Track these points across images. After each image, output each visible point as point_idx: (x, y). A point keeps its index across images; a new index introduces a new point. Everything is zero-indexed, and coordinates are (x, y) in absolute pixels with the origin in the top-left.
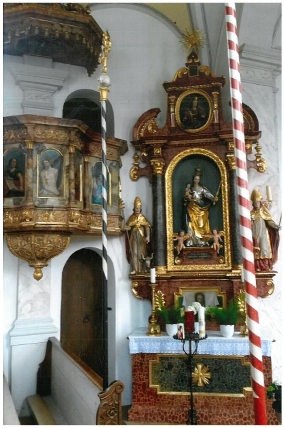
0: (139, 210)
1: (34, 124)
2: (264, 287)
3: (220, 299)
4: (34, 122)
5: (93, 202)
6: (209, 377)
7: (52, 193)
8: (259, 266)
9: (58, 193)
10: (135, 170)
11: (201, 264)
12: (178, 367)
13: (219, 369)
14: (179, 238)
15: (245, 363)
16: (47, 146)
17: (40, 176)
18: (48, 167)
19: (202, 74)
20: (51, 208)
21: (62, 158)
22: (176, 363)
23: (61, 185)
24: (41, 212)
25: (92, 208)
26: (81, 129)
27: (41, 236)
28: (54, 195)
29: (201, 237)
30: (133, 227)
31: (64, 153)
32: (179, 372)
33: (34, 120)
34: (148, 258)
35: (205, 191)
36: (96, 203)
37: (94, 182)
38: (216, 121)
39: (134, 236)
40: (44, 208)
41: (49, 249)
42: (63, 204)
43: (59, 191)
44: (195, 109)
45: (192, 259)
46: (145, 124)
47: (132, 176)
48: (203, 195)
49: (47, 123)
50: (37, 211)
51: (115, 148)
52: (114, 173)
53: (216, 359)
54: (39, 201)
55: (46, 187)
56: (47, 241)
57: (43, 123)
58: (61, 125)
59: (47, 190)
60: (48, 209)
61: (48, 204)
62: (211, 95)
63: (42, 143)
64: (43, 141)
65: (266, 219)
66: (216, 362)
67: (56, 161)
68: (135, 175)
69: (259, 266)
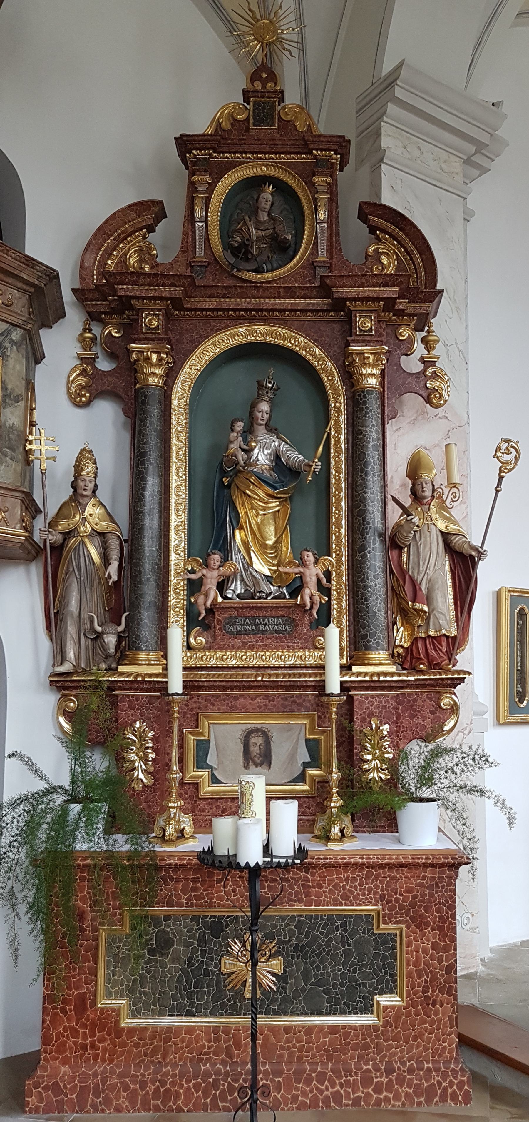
2: (431, 712)
3: (312, 747)
6: (279, 971)
10: (83, 373)
11: (266, 648)
12: (187, 945)
13: (309, 945)
14: (204, 572)
15: (382, 926)
19: (286, 125)
22: (180, 933)
29: (268, 573)
30: (67, 535)
32: (190, 959)
34: (111, 628)
35: (284, 447)
38: (322, 257)
44: (264, 217)
45: (239, 633)
48: (277, 457)
51: (19, 289)
53: (301, 916)
62: (311, 185)
65: (445, 531)
66: (300, 925)
68: (82, 387)
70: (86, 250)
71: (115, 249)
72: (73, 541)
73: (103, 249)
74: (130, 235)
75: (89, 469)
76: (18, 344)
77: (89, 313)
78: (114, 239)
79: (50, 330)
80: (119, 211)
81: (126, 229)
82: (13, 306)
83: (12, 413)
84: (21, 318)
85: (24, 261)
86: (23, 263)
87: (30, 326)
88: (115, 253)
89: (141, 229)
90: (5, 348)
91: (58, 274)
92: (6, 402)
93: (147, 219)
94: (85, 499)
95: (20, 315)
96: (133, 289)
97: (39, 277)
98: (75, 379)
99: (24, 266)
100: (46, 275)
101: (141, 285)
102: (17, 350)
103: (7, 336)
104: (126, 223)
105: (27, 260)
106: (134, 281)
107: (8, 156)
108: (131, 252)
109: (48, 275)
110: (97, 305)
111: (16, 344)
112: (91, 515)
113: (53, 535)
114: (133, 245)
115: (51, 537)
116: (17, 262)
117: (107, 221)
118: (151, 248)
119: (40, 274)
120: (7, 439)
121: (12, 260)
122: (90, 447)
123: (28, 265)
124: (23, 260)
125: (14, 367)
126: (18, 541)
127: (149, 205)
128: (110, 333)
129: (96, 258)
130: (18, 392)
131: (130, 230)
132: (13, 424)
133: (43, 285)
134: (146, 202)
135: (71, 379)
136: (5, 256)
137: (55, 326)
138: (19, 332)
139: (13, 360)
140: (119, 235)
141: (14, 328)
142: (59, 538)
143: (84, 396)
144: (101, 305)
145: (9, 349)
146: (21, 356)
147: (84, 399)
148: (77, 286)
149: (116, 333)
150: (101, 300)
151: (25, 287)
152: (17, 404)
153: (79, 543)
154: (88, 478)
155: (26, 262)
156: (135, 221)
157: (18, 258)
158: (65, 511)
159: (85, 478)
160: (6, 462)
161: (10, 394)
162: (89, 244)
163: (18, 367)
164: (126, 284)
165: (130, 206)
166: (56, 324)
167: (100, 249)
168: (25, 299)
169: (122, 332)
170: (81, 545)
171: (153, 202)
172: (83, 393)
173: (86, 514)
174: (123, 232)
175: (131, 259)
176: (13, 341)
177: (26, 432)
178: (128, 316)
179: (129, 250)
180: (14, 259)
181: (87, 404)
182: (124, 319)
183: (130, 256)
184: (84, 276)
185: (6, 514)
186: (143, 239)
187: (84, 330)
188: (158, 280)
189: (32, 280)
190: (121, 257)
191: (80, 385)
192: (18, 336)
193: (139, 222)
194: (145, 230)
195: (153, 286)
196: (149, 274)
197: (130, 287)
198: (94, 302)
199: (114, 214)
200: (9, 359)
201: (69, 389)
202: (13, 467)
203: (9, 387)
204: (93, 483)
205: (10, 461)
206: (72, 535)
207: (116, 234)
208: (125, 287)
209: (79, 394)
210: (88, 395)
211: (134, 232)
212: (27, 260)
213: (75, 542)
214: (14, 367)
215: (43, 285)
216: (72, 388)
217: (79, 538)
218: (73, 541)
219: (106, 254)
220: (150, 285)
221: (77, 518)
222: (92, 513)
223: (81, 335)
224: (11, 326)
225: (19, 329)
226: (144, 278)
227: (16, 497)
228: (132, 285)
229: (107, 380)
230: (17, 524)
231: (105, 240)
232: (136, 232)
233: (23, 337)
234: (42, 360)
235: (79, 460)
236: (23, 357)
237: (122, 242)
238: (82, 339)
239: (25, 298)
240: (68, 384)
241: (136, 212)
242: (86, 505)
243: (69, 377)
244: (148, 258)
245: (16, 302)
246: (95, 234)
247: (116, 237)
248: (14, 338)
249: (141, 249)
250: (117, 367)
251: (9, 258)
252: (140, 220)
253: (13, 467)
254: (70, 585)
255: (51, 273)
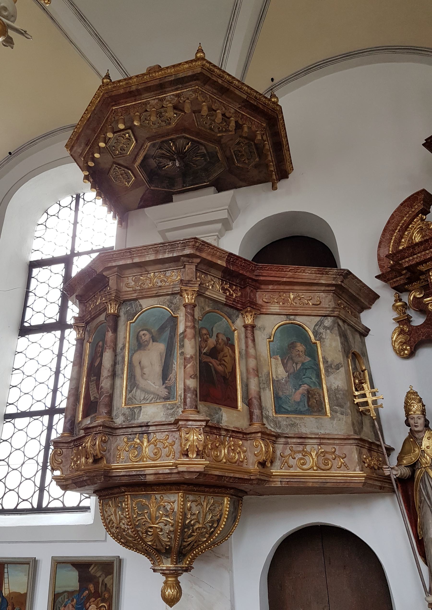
0: (421, 422)
1: (116, 269)
4: (114, 264)
5: (279, 409)
7: (154, 393)
8: (229, 289)
9: (164, 392)
10: (402, 332)
16: (146, 304)
17: (130, 363)
18: (148, 342)
20: (144, 429)
21: (174, 320)
23: (172, 376)
24: (125, 440)
25: (277, 424)
26: (204, 255)
27: (146, 496)
28: (158, 397)
30: (413, 467)
31: (177, 309)
33: (115, 261)
36: (287, 412)
37: (277, 364)
39: (420, 491)
40: (130, 430)
41: (168, 528)
42: (172, 415)
43: (166, 388)
46: (404, 234)
47: (397, 347)
49: (137, 260)
50: (118, 438)
51: (324, 291)
52: (327, 342)
54: (124, 414)
55: (142, 383)
56: (158, 509)
57: (129, 262)
58: (160, 257)
59: (144, 391)
60: (139, 429)
61: (142, 418)
63: (136, 299)
64: (135, 295)
67: (162, 329)
68: (402, 343)
69: (229, 289)
70: (379, 247)
71: (402, 238)
72: (418, 472)
73: (392, 241)
74: (411, 223)
75: (415, 407)
76: (331, 328)
77: (394, 288)
78: (399, 231)
79: (370, 310)
80: (395, 212)
81: (405, 221)
82: (322, 304)
83: (335, 379)
84: (328, 310)
85: (319, 272)
86: (318, 274)
87: (336, 313)
88: (403, 240)
89: (417, 215)
90: (321, 333)
91: (348, 271)
92: (328, 371)
93: (418, 206)
94: (420, 434)
95: (326, 308)
96: (414, 259)
97: (334, 279)
98: (396, 338)
99: (320, 275)
100: (339, 275)
101: (419, 253)
102: (331, 332)
103: (320, 325)
104: (404, 217)
105: (320, 271)
106: (411, 253)
107: (318, 216)
108: (414, 234)
109: (341, 275)
110: (397, 281)
111: (329, 328)
112: (428, 447)
113: (397, 471)
114: (415, 229)
115: (394, 472)
116: (314, 275)
117: (389, 222)
118: (429, 225)
119: (335, 276)
120: (335, 399)
121: (309, 275)
122: (415, 389)
123: (323, 274)
124: (317, 272)
125: (331, 345)
126: (358, 481)
127: (415, 197)
128: (414, 297)
129: (389, 249)
130: (337, 362)
131: (408, 220)
132: (338, 386)
133: (340, 283)
134: (412, 196)
135: (394, 339)
136: (304, 274)
137: (373, 306)
138: (329, 320)
139: (329, 340)
140: (401, 227)
141: (325, 318)
142: (406, 472)
143: (406, 349)
144: (401, 280)
145: (324, 333)
146: (334, 335)
147: (406, 352)
148: (379, 273)
149: (419, 294)
150: (399, 276)
151: (327, 288)
152: (338, 371)
153: (424, 473)
154: (415, 416)
155: (320, 272)
156: (410, 212)
157: (313, 272)
158: (407, 447)
159: (413, 416)
160: (337, 417)
161: (331, 365)
162: (380, 243)
163: (334, 344)
164: (407, 257)
165: (402, 204)
166: (374, 305)
167: (390, 242)
168: (330, 296)
169: (424, 292)
170: (426, 476)
171: (418, 193)
172: (404, 347)
173: (423, 447)
174: (403, 224)
175: (416, 239)
176: (326, 327)
177: (353, 390)
178: (423, 279)
179: (413, 233)
180: (311, 273)
181: (412, 354)
182: (422, 282)
183: (415, 238)
184: (383, 265)
185: (344, 459)
186: (421, 221)
187: (396, 301)
188: (429, 244)
189: (330, 282)
190: (409, 241)
191: (401, 342)
192: (329, 323)
193: (413, 212)
194: (420, 215)
195: (428, 250)
196: (421, 243)
197: (411, 258)
198: (395, 280)
199: (392, 215)
200: (325, 340)
201: (394, 347)
202: (344, 420)
203: (329, 360)
204: (422, 419)
205: (340, 416)
206: (417, 467)
207: (399, 227)
208: (407, 260)
209: (402, 349)
210: (408, 348)
211: (412, 220)
212: (320, 271)
213: (420, 473)
214: (331, 345)
215: (340, 283)
216: (396, 346)
217: (423, 469)
218: (418, 472)
219: (395, 243)
220: (425, 250)
221: (417, 451)
222: (428, 445)
223: (393, 305)
224: (323, 318)
225: (329, 318)
226: (418, 247)
227: (351, 444)
228: (411, 256)
229: (422, 332)
230: (356, 466)
231: (392, 235)
232: (414, 219)
233: (334, 322)
234: (368, 332)
235: (406, 403)
236: (336, 336)
237: (406, 230)
238: (395, 308)
239: (330, 295)
240: (392, 344)
241: (408, 206)
242: (422, 439)
243: (392, 338)
244: (429, 233)
245: (324, 300)
246: (383, 234)
247: (399, 230)
248: (326, 325)
249: (421, 229)
250: (426, 319)
251: (307, 274)
252: (413, 210)
253: (344, 420)
254: (425, 513)
255: (343, 272)
